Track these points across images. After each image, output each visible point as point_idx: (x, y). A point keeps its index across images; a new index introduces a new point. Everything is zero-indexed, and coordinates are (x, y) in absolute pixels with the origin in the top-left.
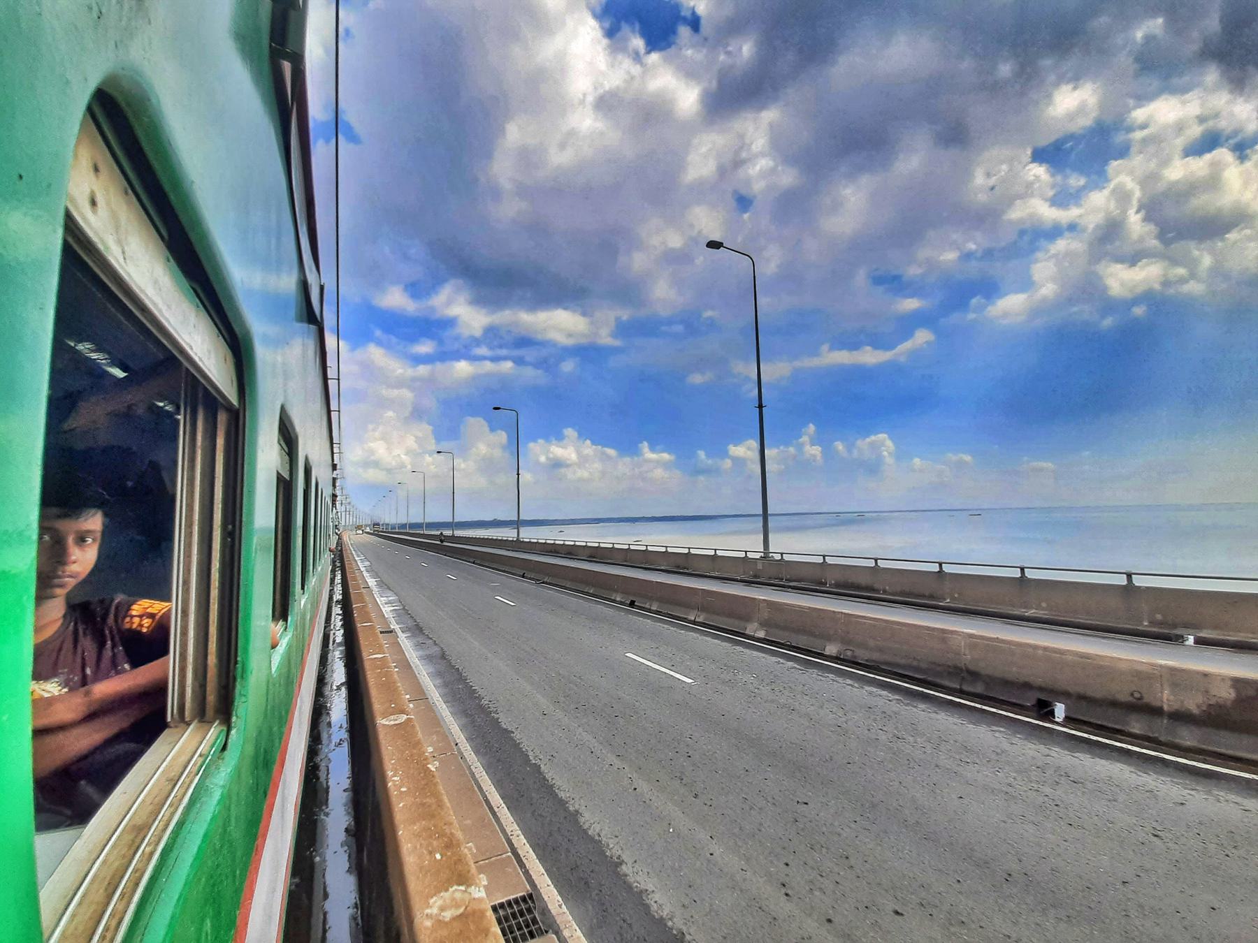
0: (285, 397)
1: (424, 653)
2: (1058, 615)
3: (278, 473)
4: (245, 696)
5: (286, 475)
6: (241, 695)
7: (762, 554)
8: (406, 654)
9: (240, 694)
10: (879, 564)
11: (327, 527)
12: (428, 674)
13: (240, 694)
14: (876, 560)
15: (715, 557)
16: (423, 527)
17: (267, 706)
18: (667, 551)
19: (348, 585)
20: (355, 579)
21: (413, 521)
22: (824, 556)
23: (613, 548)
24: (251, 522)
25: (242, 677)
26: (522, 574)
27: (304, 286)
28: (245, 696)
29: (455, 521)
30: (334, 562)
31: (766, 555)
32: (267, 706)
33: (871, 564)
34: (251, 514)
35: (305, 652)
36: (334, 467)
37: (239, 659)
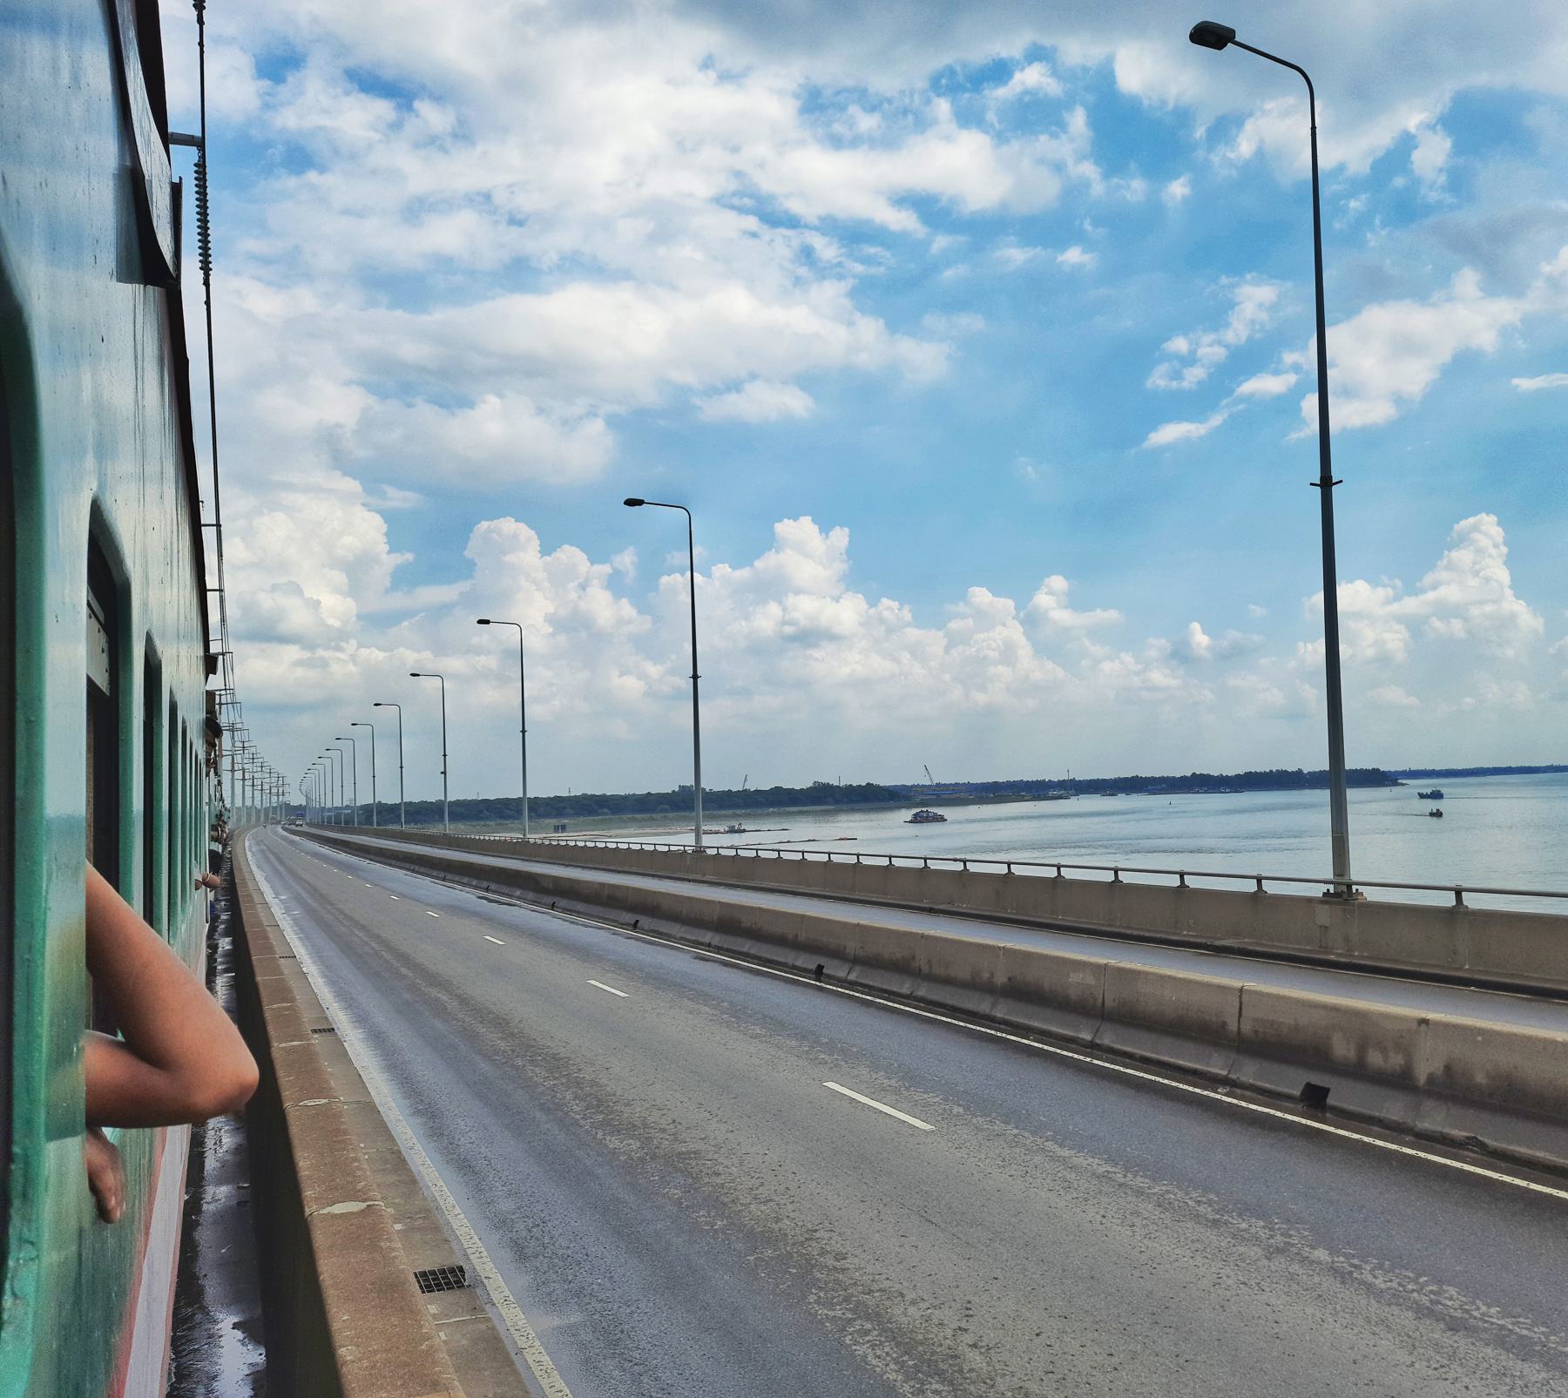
0: (101, 485)
1: (557, 1322)
2: (1422, 965)
3: (89, 679)
4: (32, 1243)
5: (102, 682)
6: (24, 1241)
7: (1331, 888)
8: (60, 522)
9: (20, 1238)
10: (1186, 883)
11: (198, 818)
12: (539, 1336)
13: (20, 1238)
14: (1458, 893)
15: (1457, 914)
16: (399, 817)
17: (80, 1274)
18: (757, 856)
19: (300, 1229)
20: (284, 993)
21: (413, 796)
22: (890, 857)
23: (669, 850)
24: (35, 801)
25: (25, 1195)
26: (813, 966)
27: (133, 183)
28: (32, 1243)
29: (530, 795)
30: (214, 919)
31: (1343, 894)
32: (80, 1274)
33: (1251, 886)
34: (34, 778)
35: (199, 943)
36: (210, 664)
37: (16, 1149)
